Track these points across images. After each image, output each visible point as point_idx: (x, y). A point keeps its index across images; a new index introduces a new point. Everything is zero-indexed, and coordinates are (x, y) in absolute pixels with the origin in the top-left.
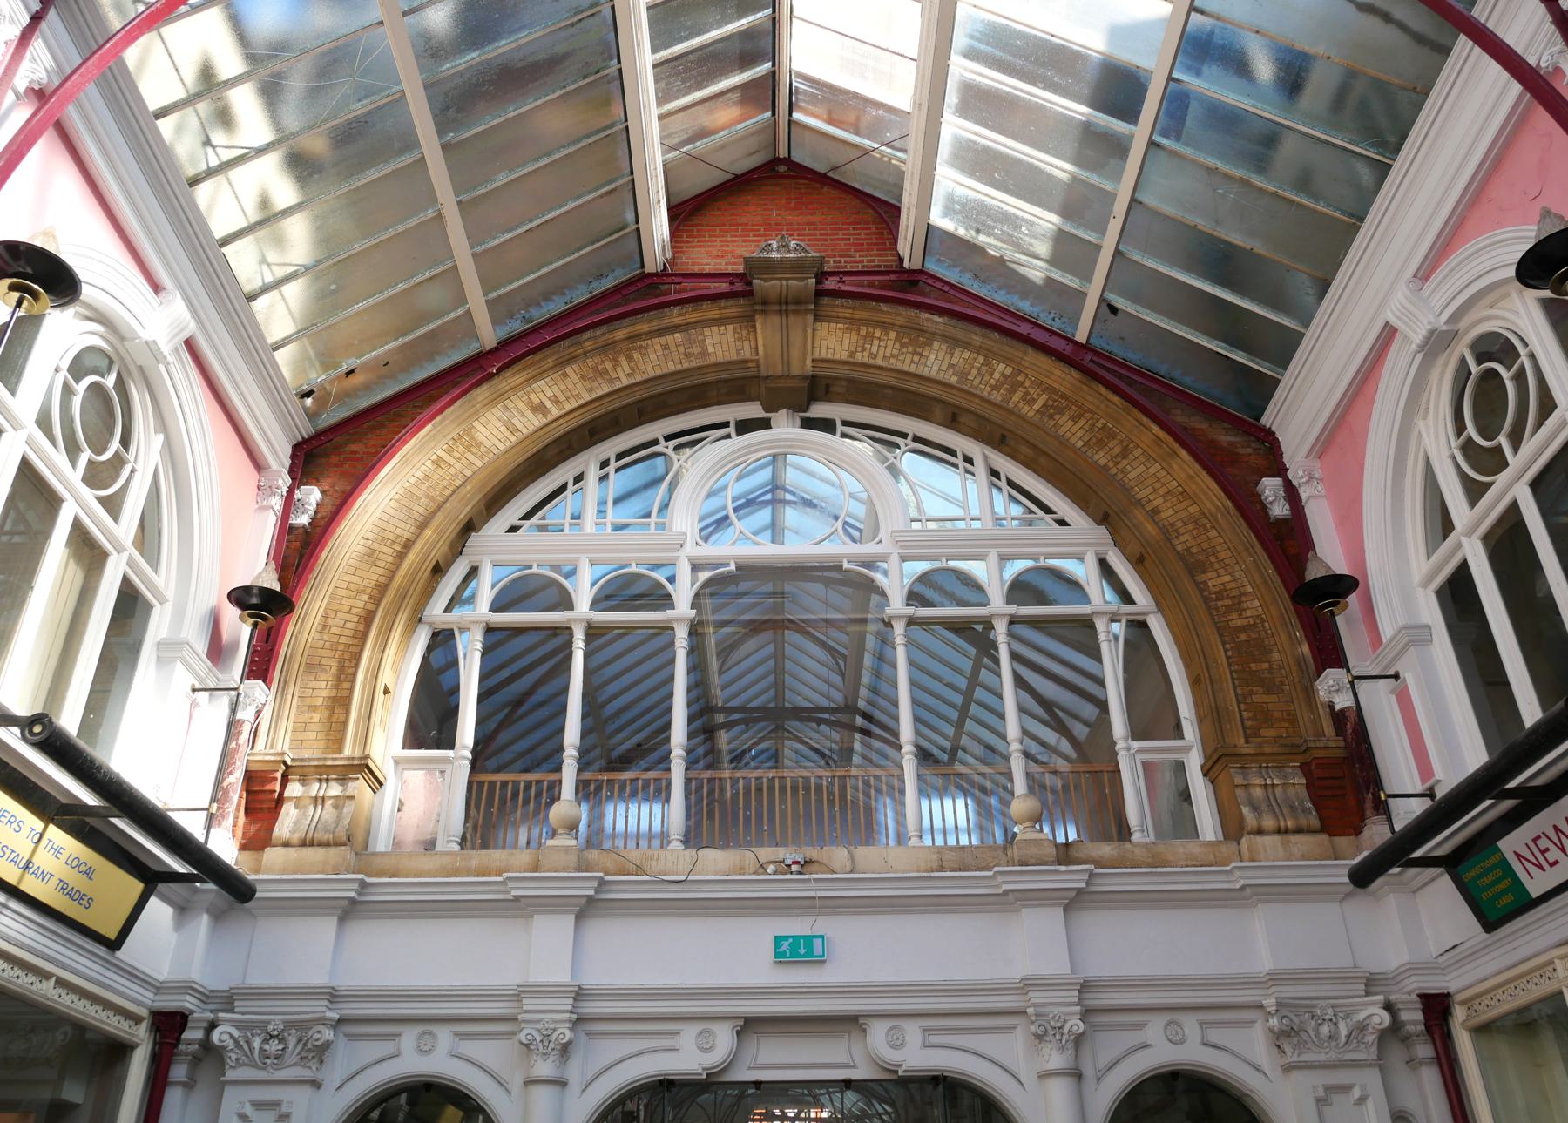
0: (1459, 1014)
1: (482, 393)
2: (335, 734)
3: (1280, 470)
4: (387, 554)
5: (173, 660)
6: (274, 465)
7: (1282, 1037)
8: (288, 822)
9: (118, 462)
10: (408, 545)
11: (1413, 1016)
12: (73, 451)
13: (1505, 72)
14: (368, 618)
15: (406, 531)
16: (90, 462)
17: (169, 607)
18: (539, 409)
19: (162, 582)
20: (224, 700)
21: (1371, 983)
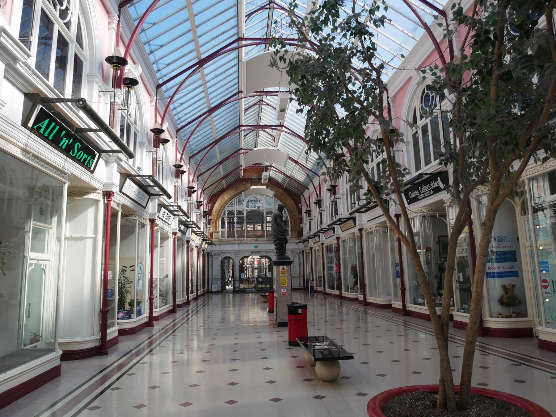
0: (340, 239)
1: (225, 193)
2: (216, 230)
3: (301, 203)
4: (218, 211)
5: (143, 146)
6: (113, 12)
7: (292, 253)
8: (214, 237)
9: (67, 9)
10: (220, 210)
11: (301, 252)
12: (55, 6)
13: (431, 39)
14: (217, 218)
15: (219, 209)
16: (60, 10)
17: (88, 62)
18: (230, 195)
19: (85, 54)
20: (108, 95)
21: (299, 249)
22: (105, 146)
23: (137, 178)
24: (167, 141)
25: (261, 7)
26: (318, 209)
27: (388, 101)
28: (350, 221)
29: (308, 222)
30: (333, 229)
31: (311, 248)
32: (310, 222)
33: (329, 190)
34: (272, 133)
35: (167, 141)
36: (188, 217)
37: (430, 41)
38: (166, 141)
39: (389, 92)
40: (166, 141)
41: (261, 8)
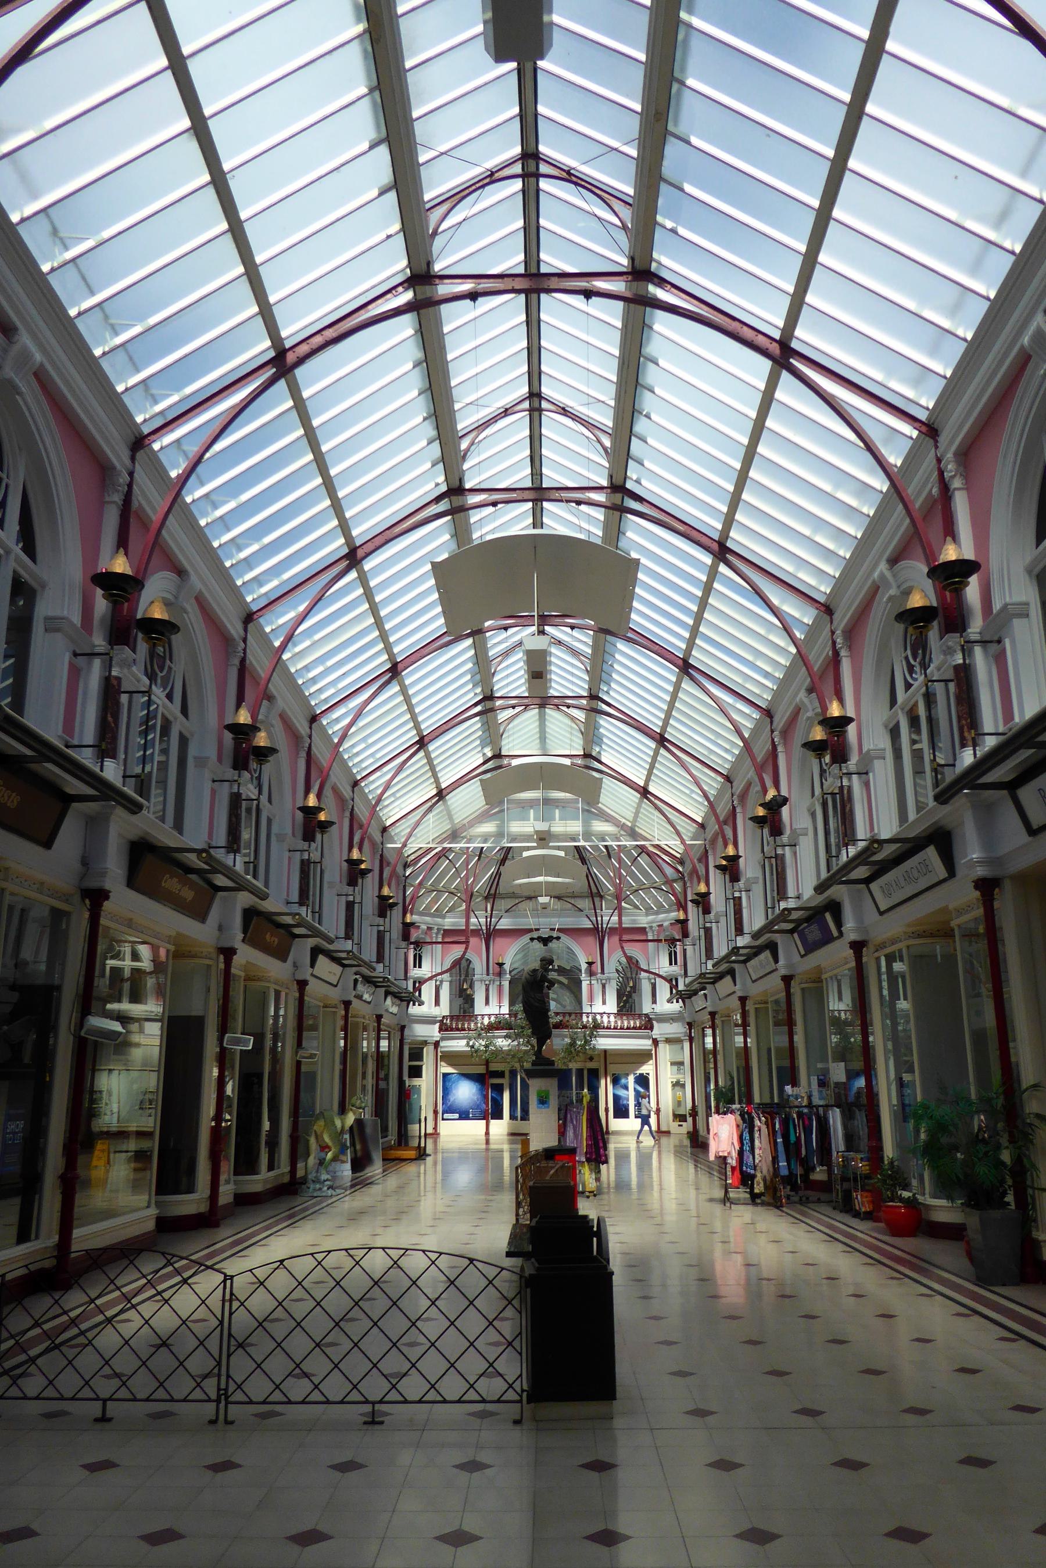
29: (702, 932)
30: (772, 948)
32: (708, 932)
33: (759, 821)
38: (263, 754)
41: (506, 412)
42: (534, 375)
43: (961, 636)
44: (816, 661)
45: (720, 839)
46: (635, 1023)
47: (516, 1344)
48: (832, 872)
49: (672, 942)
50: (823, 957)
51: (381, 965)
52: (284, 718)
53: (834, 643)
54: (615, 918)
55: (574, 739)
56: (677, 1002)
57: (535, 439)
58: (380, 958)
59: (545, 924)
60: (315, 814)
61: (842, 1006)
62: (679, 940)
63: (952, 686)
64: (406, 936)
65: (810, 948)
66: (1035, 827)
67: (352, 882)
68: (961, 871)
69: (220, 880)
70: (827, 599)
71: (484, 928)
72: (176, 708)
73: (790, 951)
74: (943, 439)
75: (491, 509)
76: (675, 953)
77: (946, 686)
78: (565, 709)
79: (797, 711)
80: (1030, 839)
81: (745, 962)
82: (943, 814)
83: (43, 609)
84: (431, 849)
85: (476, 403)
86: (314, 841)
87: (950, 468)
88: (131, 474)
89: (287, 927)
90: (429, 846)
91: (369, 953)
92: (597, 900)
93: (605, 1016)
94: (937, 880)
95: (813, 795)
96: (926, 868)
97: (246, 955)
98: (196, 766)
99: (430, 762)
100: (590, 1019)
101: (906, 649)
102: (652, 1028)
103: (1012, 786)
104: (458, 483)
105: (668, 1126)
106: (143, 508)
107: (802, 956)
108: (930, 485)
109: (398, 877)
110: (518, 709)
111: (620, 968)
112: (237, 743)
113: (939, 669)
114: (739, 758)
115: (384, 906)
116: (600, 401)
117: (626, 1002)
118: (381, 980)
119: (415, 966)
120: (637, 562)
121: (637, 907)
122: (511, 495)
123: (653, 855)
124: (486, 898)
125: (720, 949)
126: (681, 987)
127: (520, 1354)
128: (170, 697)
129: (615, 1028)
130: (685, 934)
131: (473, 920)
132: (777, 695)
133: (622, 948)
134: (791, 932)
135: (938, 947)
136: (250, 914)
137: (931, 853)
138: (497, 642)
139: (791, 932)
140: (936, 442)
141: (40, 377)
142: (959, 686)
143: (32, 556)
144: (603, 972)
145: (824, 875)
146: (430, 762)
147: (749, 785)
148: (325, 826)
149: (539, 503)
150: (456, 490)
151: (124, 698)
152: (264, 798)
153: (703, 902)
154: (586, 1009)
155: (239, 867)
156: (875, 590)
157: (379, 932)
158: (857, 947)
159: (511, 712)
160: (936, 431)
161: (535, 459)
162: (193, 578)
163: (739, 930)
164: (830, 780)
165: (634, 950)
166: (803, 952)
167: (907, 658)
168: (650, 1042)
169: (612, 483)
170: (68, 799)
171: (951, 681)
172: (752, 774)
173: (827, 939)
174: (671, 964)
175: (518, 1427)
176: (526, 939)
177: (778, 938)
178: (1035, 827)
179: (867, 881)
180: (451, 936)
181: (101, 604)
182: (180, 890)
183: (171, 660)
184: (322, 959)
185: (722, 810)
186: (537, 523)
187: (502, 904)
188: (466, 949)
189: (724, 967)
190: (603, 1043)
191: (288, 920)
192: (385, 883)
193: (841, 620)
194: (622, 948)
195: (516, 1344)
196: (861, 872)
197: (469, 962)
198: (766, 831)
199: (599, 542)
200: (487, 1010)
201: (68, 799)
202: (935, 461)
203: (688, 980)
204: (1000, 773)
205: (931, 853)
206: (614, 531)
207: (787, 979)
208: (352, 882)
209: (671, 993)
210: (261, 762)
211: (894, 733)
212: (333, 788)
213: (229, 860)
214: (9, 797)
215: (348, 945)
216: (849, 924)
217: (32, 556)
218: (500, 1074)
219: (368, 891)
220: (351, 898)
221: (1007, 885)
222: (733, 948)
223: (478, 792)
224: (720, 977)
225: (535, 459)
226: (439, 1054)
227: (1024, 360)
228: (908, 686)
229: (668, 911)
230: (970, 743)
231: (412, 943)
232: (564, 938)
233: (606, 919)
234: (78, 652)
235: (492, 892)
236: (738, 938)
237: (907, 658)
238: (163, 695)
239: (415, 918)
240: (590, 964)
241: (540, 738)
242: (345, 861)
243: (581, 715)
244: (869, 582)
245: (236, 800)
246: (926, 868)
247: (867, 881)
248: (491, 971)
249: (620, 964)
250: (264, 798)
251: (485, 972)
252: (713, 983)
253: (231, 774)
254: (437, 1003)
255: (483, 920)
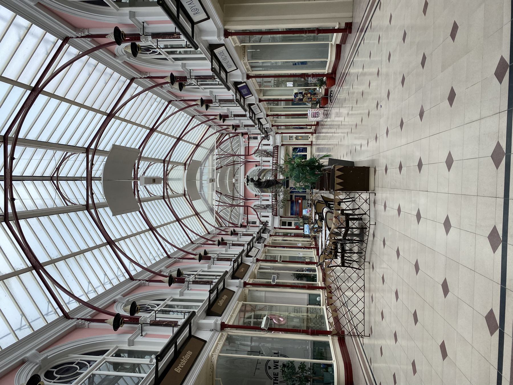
22: (187, 330)
23: (174, 345)
24: (179, 271)
25: (57, 189)
26: (229, 118)
27: (179, 101)
28: (253, 109)
29: (246, 128)
30: (250, 105)
31: (249, 77)
32: (245, 126)
33: (207, 107)
34: (142, 169)
35: (179, 271)
36: (226, 272)
37: (155, 89)
38: (179, 273)
39: (172, 100)
40: (179, 273)
41: (58, 188)
42: (42, 178)
43: (141, 35)
44: (152, 84)
45: (214, 120)
46: (276, 152)
47: (360, 194)
48: (223, 84)
49: (249, 138)
50: (253, 89)
51: (254, 235)
52: (167, 267)
53: (144, 78)
54: (242, 157)
55: (179, 168)
56: (269, 137)
57: (67, 179)
58: (251, 235)
59: (242, 180)
60: (201, 256)
61: (273, 82)
62: (249, 136)
63: (159, 40)
64: (245, 226)
65: (250, 93)
66: (207, 17)
67: (225, 244)
68: (222, 42)
69: (221, 286)
70: (129, 79)
71: (244, 201)
72: (162, 303)
73: (251, 99)
74: (69, 35)
75: (94, 195)
76: (253, 137)
77: (159, 41)
78: (168, 172)
79: (169, 92)
80: (211, 19)
81: (255, 114)
82: (202, 48)
83: (126, 347)
84: (216, 217)
85: (54, 200)
86: (211, 256)
87: (79, 35)
88: (78, 319)
89: (238, 266)
90: (215, 218)
91: (249, 238)
92: (235, 163)
93: (274, 161)
94: (225, 50)
95: (199, 88)
96: (221, 53)
97: (247, 279)
98: (183, 296)
99: (185, 218)
100: (274, 166)
101: (147, 54)
102: (278, 146)
103: (193, 23)
104: (85, 207)
105: (310, 142)
106: (91, 315)
107: (252, 96)
108: (87, 41)
109: (225, 229)
110: (168, 187)
111: (259, 156)
112: (175, 282)
113: (153, 43)
114: (185, 112)
115: (234, 233)
116: (54, 154)
117: (270, 154)
118: (258, 235)
119: (256, 224)
120: (114, 146)
121: (238, 150)
122: (89, 188)
123: (219, 142)
124: (233, 200)
125: (251, 123)
126: (264, 136)
127: (362, 193)
128: (158, 305)
129: (277, 158)
130: (246, 134)
131: (241, 204)
132: (163, 97)
133: (251, 155)
134: (244, 99)
135: (248, 50)
136: (233, 277)
137: (216, 51)
138: (143, 194)
139: (244, 99)
140: (70, 38)
141: (41, 350)
142: (159, 38)
143: (106, 351)
144: (259, 162)
145: (223, 86)
146: (185, 218)
147: (195, 109)
148: (206, 253)
149: (92, 178)
150: (87, 207)
151: (158, 319)
152: (195, 273)
153: (235, 127)
154: (271, 168)
155: (216, 280)
156: (125, 62)
157: (243, 235)
158: (249, 77)
159: (169, 190)
160: (66, 37)
161: (74, 179)
162: (117, 297)
163: (245, 116)
164: (193, 82)
165: (252, 151)
166: (251, 95)
167: (150, 53)
168: (282, 147)
169: (85, 152)
170: (190, 336)
171: (157, 40)
172: (192, 109)
173: (246, 87)
174: (257, 139)
175: (376, 194)
176: (248, 187)
177: (247, 102)
178: (207, 17)
179: (226, 73)
180: (246, 213)
181: (125, 327)
182: (224, 300)
183: (145, 305)
184: (250, 254)
185: (204, 119)
186: (99, 179)
187: (236, 195)
188: (250, 207)
189: (257, 122)
190: (282, 162)
191: (236, 264)
192: (227, 233)
193: (137, 75)
194: (251, 155)
195: (360, 194)
196: (223, 75)
197: (255, 206)
198: (211, 105)
199: (106, 158)
200: (271, 200)
201: (190, 336)
202: (78, 39)
203: (262, 134)
204: (188, 27)
205: (216, 51)
206: (103, 153)
207: (260, 101)
208: (225, 244)
209: (265, 139)
210: (182, 274)
211: (176, 59)
212: (193, 251)
213: (214, 284)
214: (188, 354)
215: (246, 245)
216: (240, 80)
217: (106, 351)
218: (291, 196)
219: (228, 238)
220: (231, 244)
221: (227, 27)
222: (250, 118)
223: (196, 202)
224: (259, 122)
225: (74, 179)
226: (284, 216)
227: (39, 5)
228: (160, 54)
229: (240, 139)
230: (179, 36)
231: (247, 225)
232: (248, 174)
233: (242, 160)
234: (141, 334)
235: (232, 198)
236: (247, 116)
237: (150, 53)
238: (157, 307)
239: (240, 224)
240: (256, 166)
241: (179, 180)
242: (218, 246)
243: (170, 166)
244: (122, 64)
245: (195, 282)
246: (221, 53)
247: (226, 73)
248: (258, 199)
249: (257, 156)
250: (195, 273)
251: (258, 201)
252: (262, 125)
253: (186, 283)
254: (268, 217)
255: (241, 201)
